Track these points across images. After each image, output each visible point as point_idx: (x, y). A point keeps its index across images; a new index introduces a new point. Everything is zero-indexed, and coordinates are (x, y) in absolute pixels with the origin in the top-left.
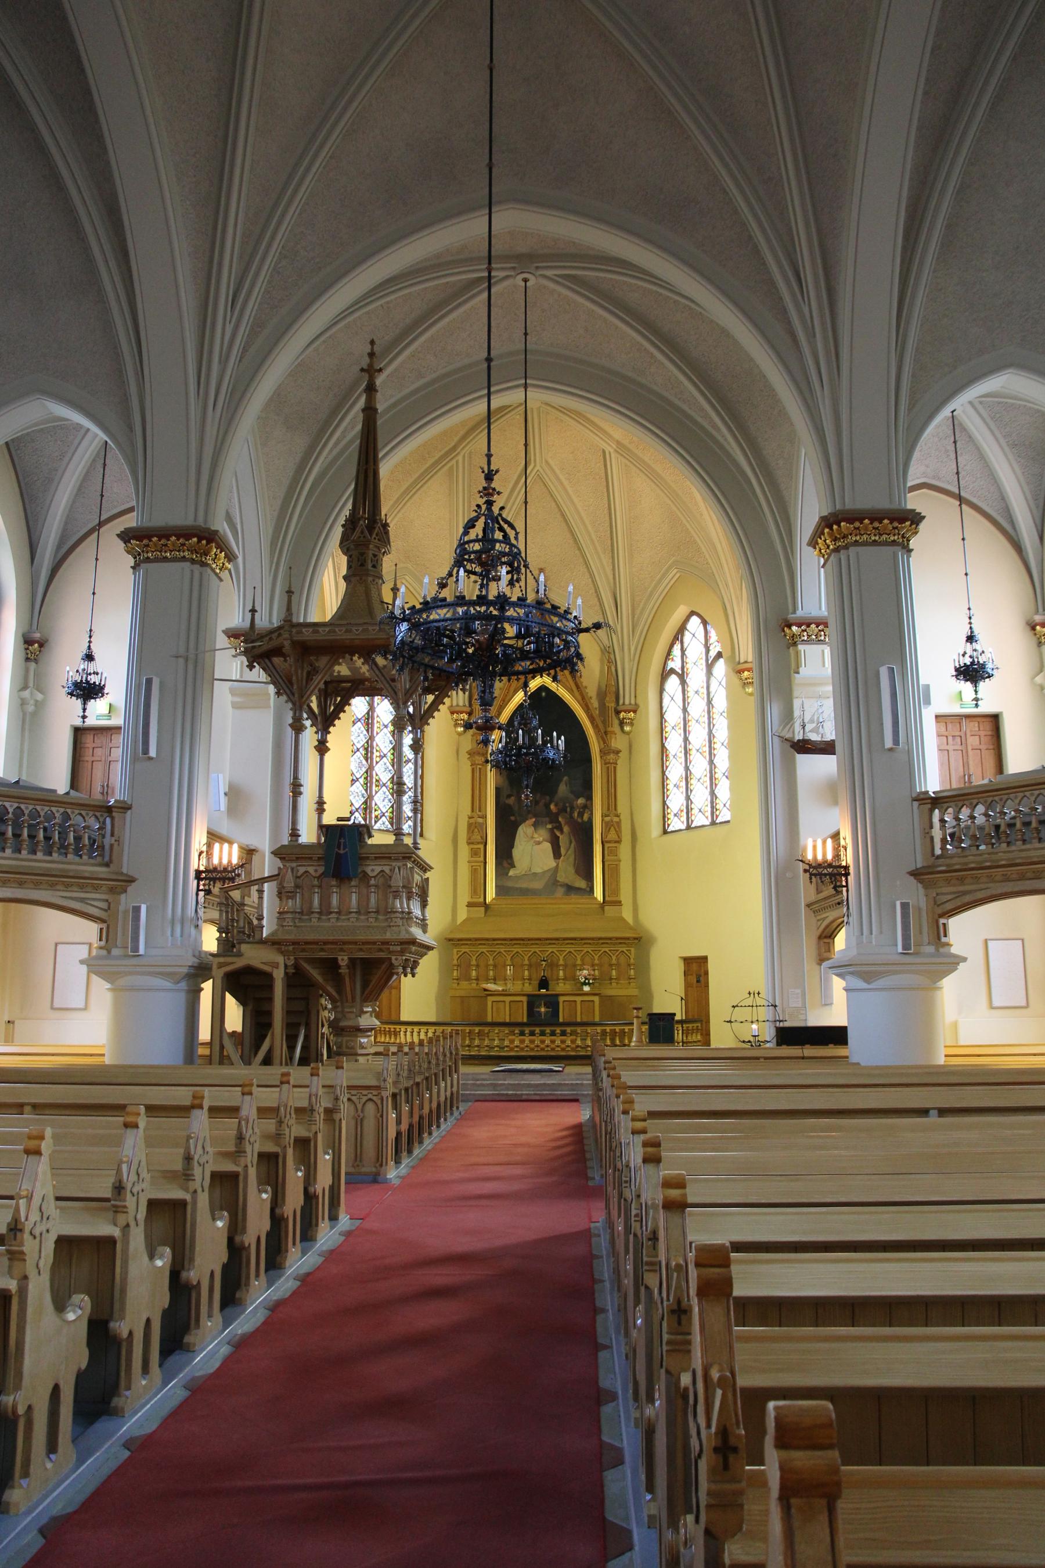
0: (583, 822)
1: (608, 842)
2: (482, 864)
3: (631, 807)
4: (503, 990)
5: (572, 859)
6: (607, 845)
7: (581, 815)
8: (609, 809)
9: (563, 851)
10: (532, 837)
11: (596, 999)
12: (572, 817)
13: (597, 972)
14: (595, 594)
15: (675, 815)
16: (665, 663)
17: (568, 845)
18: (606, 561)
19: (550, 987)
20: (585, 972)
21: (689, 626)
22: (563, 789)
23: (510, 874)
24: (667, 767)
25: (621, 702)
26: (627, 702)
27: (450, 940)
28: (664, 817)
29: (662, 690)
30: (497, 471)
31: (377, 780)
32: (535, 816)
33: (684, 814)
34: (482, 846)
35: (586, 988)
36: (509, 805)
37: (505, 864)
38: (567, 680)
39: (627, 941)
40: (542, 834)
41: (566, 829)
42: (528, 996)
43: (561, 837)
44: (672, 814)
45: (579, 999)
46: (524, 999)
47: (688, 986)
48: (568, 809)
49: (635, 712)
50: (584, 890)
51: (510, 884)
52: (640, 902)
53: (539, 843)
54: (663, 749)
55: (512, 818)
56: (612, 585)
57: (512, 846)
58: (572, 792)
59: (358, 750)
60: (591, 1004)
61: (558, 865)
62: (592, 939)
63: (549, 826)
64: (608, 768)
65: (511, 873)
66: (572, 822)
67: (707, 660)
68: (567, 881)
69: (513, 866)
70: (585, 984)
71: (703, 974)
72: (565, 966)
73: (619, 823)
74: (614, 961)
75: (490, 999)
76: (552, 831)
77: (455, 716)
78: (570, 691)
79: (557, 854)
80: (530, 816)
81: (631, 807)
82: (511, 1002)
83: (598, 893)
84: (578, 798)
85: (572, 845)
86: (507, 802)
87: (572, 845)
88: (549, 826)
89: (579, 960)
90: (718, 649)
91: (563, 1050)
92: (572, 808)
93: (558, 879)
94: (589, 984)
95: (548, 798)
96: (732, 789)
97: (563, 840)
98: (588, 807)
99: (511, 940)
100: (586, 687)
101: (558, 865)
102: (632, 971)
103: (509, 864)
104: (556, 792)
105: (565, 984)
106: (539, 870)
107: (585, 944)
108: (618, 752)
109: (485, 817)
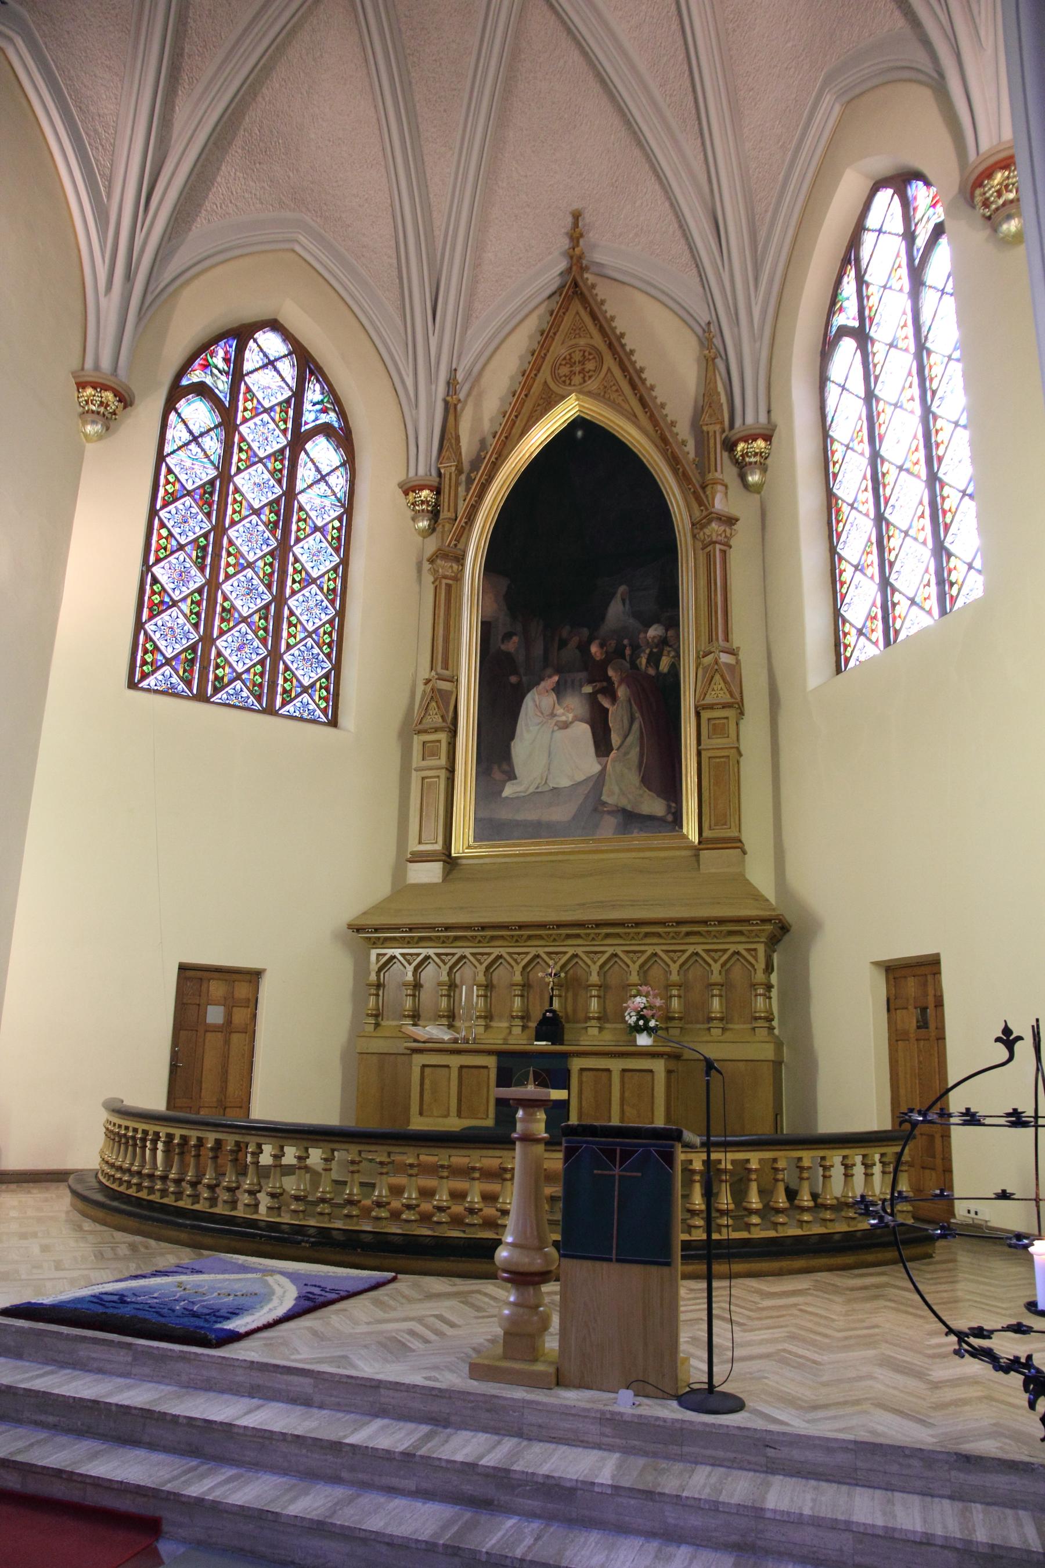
0: (659, 674)
1: (711, 707)
2: (443, 774)
3: (767, 637)
4: (455, 1041)
5: (634, 754)
6: (705, 715)
7: (654, 660)
8: (710, 641)
9: (615, 739)
10: (553, 715)
11: (659, 1066)
12: (634, 666)
13: (675, 1003)
14: (678, 233)
15: (860, 633)
16: (828, 323)
17: (626, 723)
18: (691, 147)
19: (567, 1037)
20: (640, 1001)
21: (873, 220)
22: (616, 611)
23: (505, 794)
24: (839, 535)
25: (738, 423)
26: (750, 420)
27: (359, 930)
28: (837, 644)
29: (823, 380)
30: (898, 603)
31: (224, 609)
32: (558, 671)
33: (879, 625)
34: (443, 737)
35: (643, 1040)
36: (508, 655)
37: (497, 775)
38: (626, 400)
39: (745, 928)
40: (573, 706)
41: (622, 692)
42: (500, 1054)
43: (612, 709)
44: (854, 632)
45: (616, 1065)
46: (491, 1062)
47: (896, 1037)
48: (628, 652)
49: (768, 438)
50: (662, 820)
51: (504, 814)
52: (787, 841)
53: (565, 726)
54: (830, 497)
55: (513, 679)
56: (708, 197)
57: (512, 736)
58: (636, 615)
59: (181, 547)
60: (648, 1076)
61: (604, 769)
62: (662, 923)
63: (588, 689)
64: (708, 554)
65: (509, 791)
66: (634, 678)
67: (910, 258)
68: (624, 803)
69: (511, 776)
70: (637, 1029)
71: (931, 1005)
72: (603, 987)
73: (735, 669)
74: (716, 977)
75: (419, 1060)
76: (592, 698)
77: (412, 495)
78: (633, 418)
79: (602, 745)
80: (549, 671)
81: (767, 637)
82: (462, 1067)
83: (691, 830)
84: (648, 626)
85: (636, 726)
86: (503, 647)
87: (636, 726)
88: (588, 689)
89: (634, 974)
90: (939, 214)
91: (456, 1221)
92: (636, 648)
93: (604, 798)
94: (646, 1029)
95: (585, 632)
96: (983, 529)
97: (617, 715)
98: (670, 643)
99: (483, 927)
100: (663, 406)
101: (604, 769)
102: (760, 999)
103: (504, 772)
104: (603, 618)
105: (601, 1029)
106: (565, 783)
107: (647, 935)
108: (731, 521)
109: (454, 680)
